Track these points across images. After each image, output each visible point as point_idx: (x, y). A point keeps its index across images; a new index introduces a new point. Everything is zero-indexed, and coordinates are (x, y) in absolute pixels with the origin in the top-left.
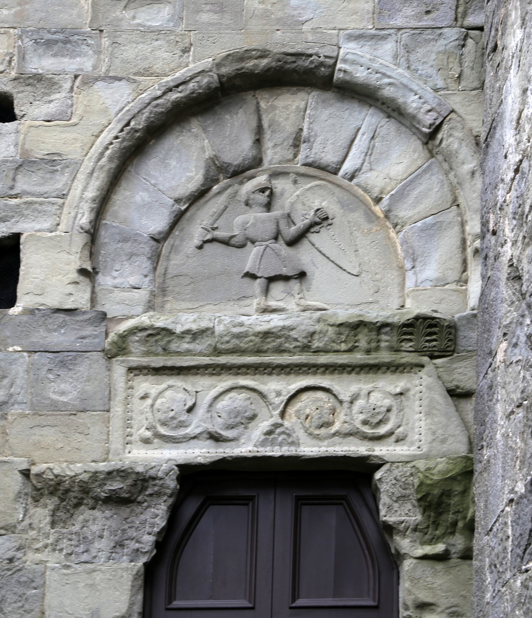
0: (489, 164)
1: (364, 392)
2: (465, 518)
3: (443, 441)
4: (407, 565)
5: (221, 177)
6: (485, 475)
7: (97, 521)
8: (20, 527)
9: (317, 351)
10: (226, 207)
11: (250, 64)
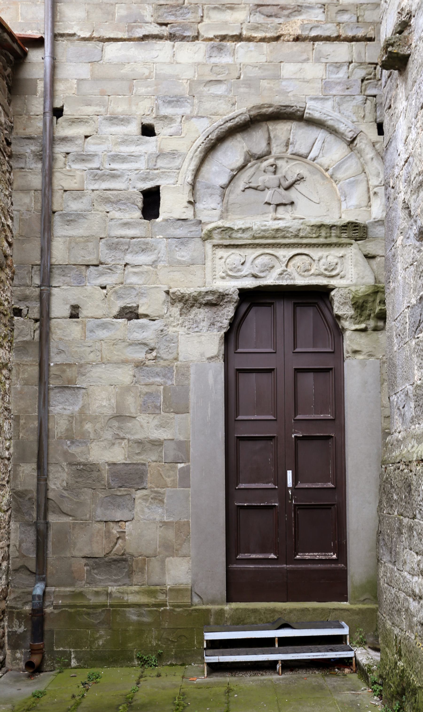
0: (388, 157)
1: (325, 256)
2: (374, 312)
3: (363, 278)
4: (347, 334)
5: (252, 159)
6: (392, 295)
7: (202, 314)
8: (165, 316)
9: (302, 238)
10: (255, 173)
11: (264, 110)
